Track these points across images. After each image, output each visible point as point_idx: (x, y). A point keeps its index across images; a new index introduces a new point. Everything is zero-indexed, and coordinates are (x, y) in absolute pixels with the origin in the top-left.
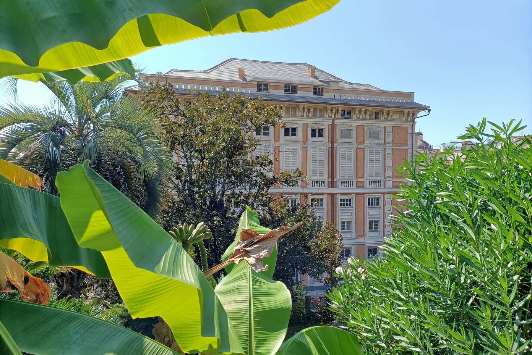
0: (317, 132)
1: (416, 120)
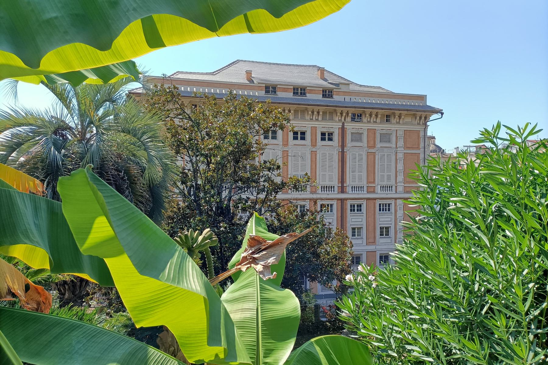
0: (326, 136)
1: (428, 123)
